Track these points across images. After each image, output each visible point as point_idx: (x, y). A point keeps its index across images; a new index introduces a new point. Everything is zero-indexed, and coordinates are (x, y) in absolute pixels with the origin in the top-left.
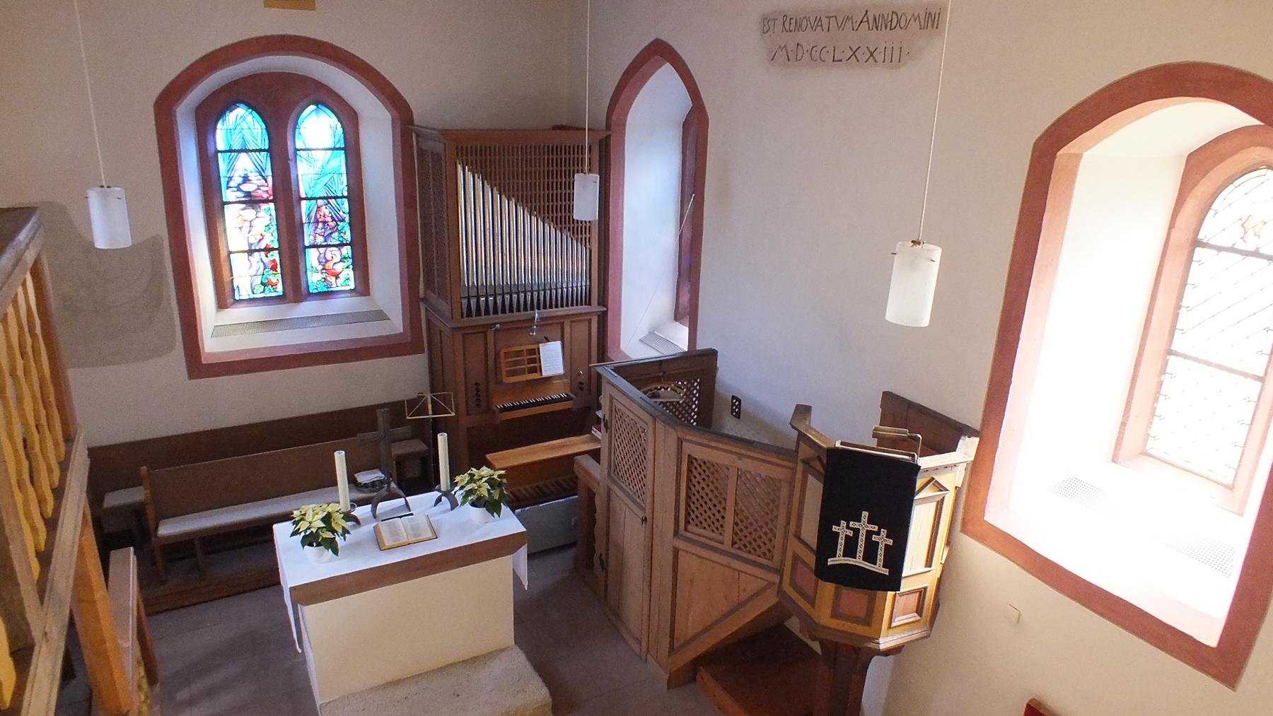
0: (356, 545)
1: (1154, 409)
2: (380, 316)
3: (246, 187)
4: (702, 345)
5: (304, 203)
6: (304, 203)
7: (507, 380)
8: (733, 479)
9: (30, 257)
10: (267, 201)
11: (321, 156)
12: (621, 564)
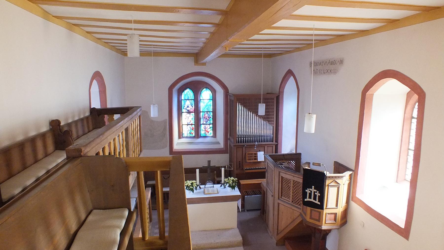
0: (199, 193)
1: (406, 166)
2: (218, 143)
3: (188, 109)
4: (298, 152)
7: (248, 161)
8: (292, 183)
9: (139, 114)
10: (192, 112)
11: (206, 101)
12: (269, 211)
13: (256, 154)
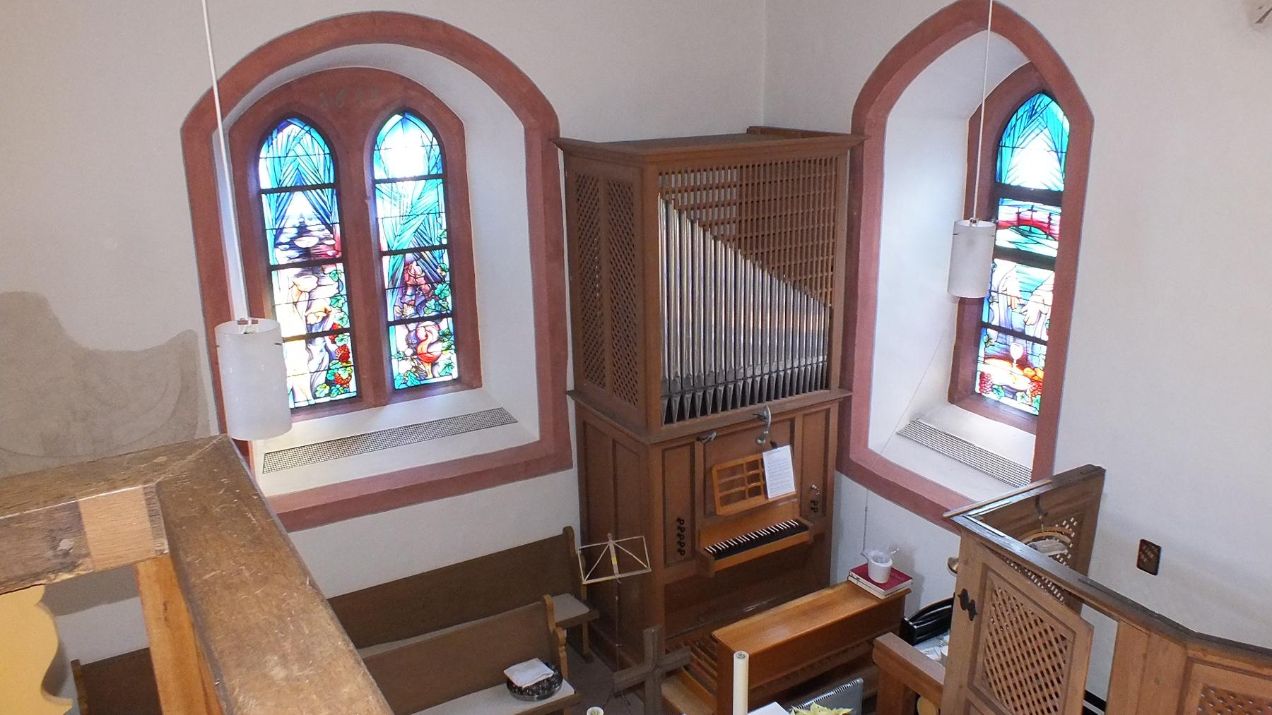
2: (500, 417)
3: (303, 243)
4: (1064, 463)
5: (386, 259)
6: (386, 259)
7: (723, 511)
10: (333, 261)
11: (409, 190)
13: (758, 464)
